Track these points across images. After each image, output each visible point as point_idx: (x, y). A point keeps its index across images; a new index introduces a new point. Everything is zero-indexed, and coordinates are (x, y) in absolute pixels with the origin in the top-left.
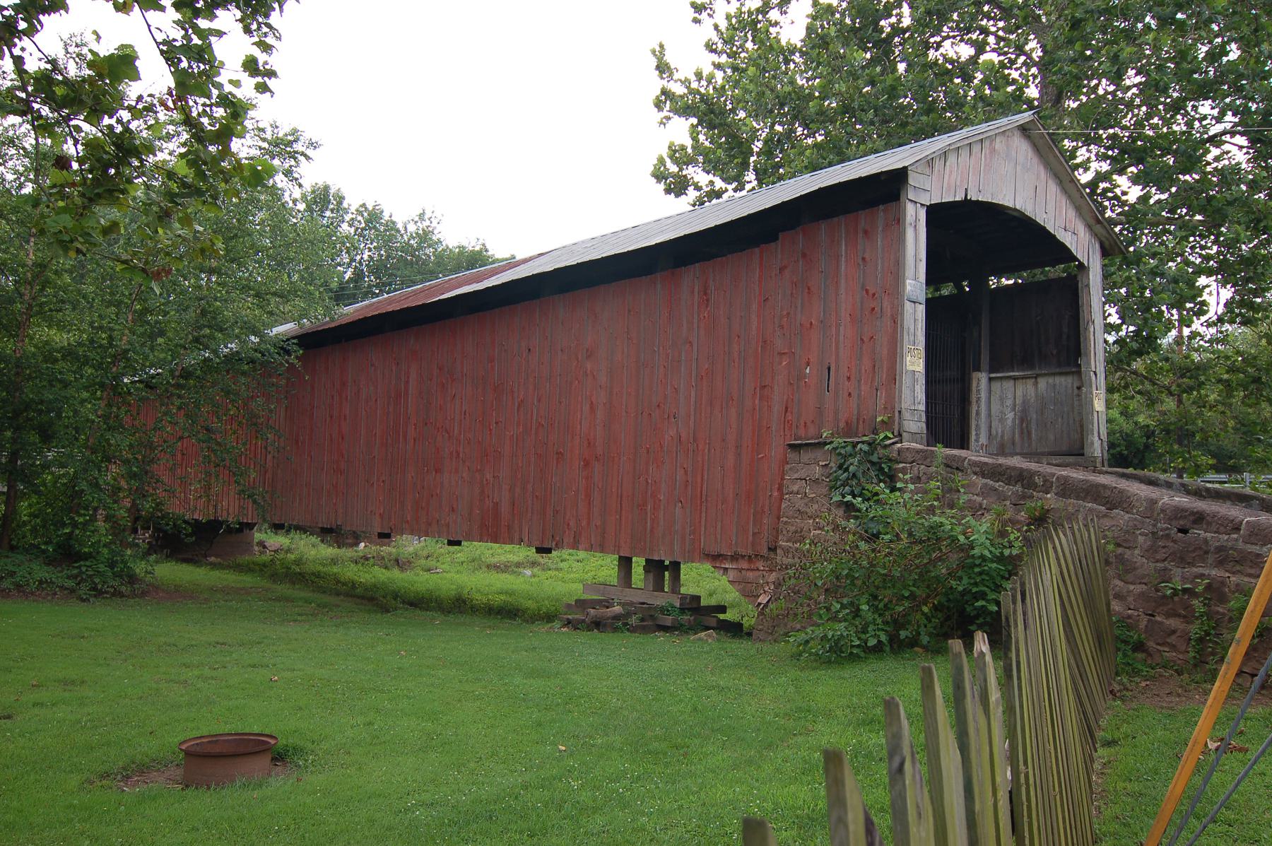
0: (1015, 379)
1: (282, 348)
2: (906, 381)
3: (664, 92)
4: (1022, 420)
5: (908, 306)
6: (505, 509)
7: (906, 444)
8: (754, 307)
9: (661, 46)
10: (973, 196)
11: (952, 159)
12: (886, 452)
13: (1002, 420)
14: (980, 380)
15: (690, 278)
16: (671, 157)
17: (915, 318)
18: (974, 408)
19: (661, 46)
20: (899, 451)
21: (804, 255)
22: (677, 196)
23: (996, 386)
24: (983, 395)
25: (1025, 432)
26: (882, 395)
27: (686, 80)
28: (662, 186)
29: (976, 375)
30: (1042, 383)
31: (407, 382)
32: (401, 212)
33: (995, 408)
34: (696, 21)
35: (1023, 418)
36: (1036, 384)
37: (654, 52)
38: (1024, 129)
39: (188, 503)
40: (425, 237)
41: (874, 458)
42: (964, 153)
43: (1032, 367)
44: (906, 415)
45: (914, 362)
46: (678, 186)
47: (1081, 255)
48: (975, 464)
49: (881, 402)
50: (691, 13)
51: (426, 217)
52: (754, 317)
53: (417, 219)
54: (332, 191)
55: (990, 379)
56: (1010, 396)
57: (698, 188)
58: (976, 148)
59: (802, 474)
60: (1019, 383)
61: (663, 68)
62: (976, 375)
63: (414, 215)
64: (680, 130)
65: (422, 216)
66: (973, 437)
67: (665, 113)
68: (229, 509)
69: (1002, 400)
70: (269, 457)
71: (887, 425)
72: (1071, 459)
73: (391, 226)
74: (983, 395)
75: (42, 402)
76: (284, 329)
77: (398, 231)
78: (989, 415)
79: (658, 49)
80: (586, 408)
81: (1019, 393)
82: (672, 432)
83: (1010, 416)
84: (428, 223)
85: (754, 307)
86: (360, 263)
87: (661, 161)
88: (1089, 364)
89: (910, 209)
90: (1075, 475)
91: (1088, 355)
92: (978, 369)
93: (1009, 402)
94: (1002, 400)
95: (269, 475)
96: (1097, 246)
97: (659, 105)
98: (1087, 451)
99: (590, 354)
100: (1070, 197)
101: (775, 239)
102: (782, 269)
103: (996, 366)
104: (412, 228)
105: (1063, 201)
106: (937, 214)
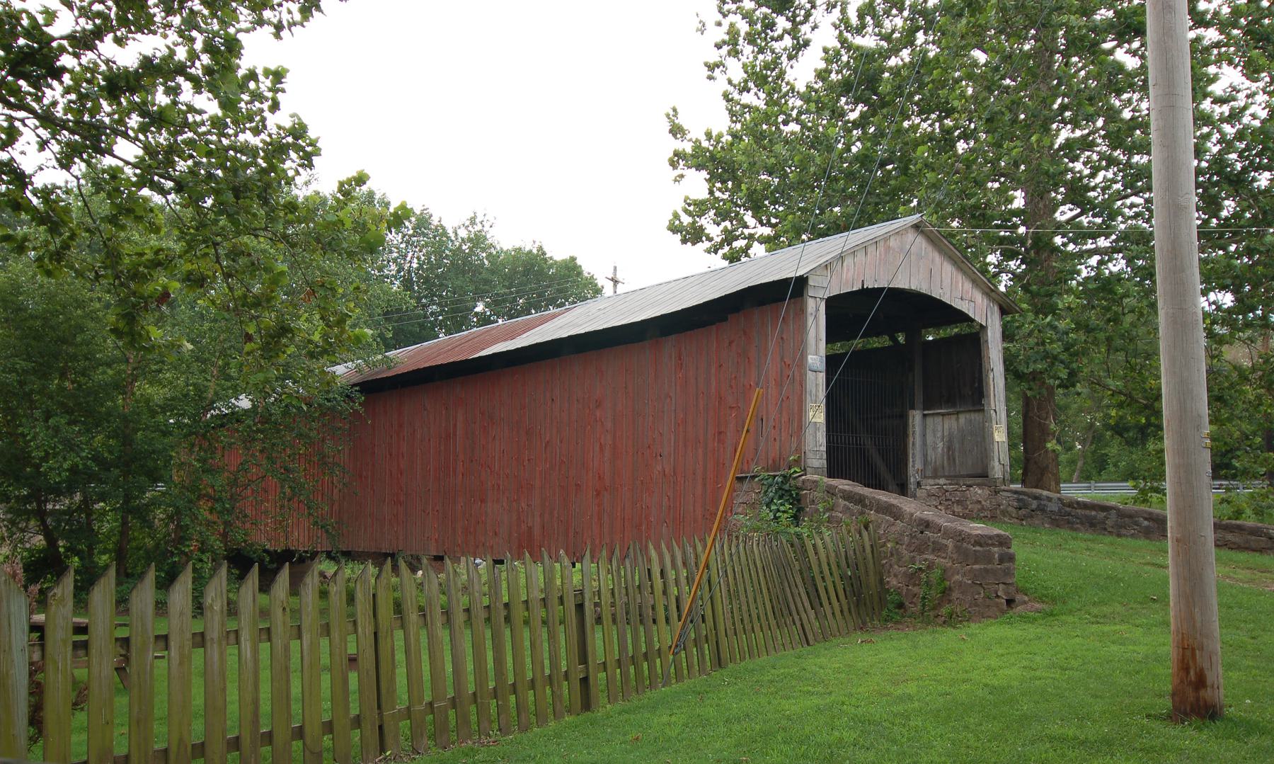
0: (943, 415)
1: (348, 396)
2: (809, 433)
3: (676, 154)
4: (949, 448)
5: (810, 375)
6: (537, 531)
7: (808, 477)
8: (713, 371)
9: (675, 110)
10: (870, 285)
11: (848, 261)
12: (793, 482)
13: (935, 448)
14: (915, 417)
15: (669, 346)
16: (686, 211)
17: (817, 383)
18: (911, 439)
19: (675, 110)
20: (804, 481)
21: (745, 333)
22: (694, 244)
23: (929, 420)
24: (918, 429)
25: (951, 459)
26: (794, 439)
27: (697, 140)
28: (678, 237)
29: (912, 413)
30: (962, 418)
31: (455, 426)
32: (451, 217)
33: (929, 439)
34: (710, 78)
35: (950, 448)
36: (957, 419)
37: (668, 116)
38: (916, 227)
39: (263, 538)
40: (478, 241)
41: (787, 487)
42: (860, 256)
43: (954, 405)
44: (810, 455)
45: (817, 416)
46: (693, 235)
47: (979, 319)
48: (843, 491)
49: (794, 446)
50: (706, 72)
51: (478, 221)
52: (713, 379)
53: (468, 223)
54: (377, 197)
55: (925, 416)
56: (940, 428)
57: (710, 239)
58: (871, 249)
59: (744, 499)
60: (946, 418)
61: (677, 131)
62: (912, 413)
63: (464, 218)
64: (697, 184)
65: (473, 221)
66: (911, 464)
67: (678, 172)
68: (299, 540)
69: (934, 432)
70: (335, 491)
71: (797, 462)
72: (979, 480)
73: (441, 232)
74: (918, 429)
75: (154, 452)
76: (341, 370)
77: (448, 238)
78: (924, 443)
79: (671, 113)
80: (597, 448)
81: (946, 426)
82: (659, 468)
83: (940, 445)
84: (478, 227)
85: (713, 371)
86: (409, 271)
87: (676, 216)
88: (989, 404)
89: (810, 304)
90: (884, 499)
91: (989, 396)
92: (913, 408)
93: (939, 434)
94: (934, 432)
95: (336, 507)
96: (996, 308)
97: (673, 164)
98: (991, 474)
99: (599, 404)
100: (964, 273)
101: (725, 319)
102: (730, 343)
103: (929, 404)
104: (463, 233)
105: (959, 277)
106: (834, 304)
